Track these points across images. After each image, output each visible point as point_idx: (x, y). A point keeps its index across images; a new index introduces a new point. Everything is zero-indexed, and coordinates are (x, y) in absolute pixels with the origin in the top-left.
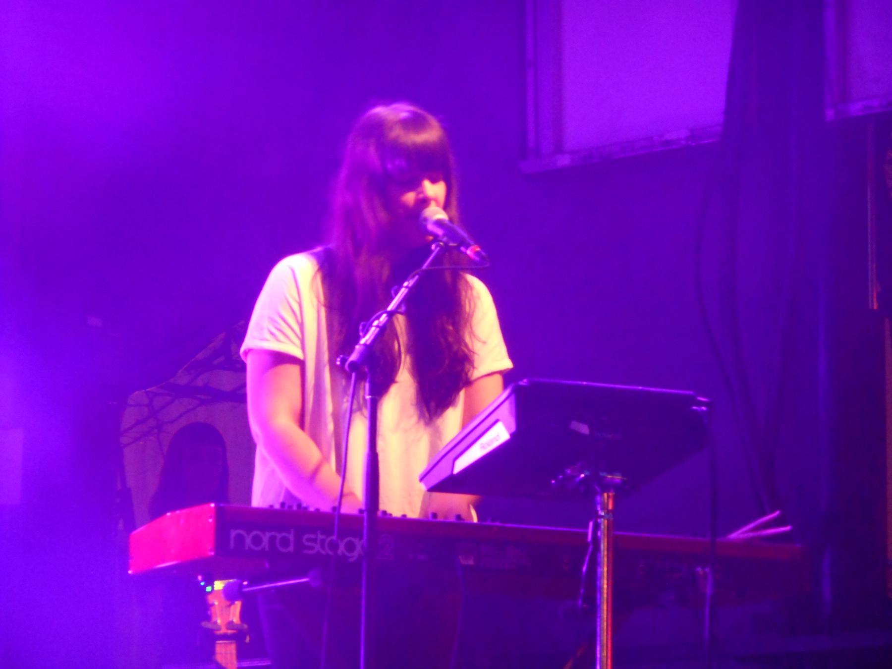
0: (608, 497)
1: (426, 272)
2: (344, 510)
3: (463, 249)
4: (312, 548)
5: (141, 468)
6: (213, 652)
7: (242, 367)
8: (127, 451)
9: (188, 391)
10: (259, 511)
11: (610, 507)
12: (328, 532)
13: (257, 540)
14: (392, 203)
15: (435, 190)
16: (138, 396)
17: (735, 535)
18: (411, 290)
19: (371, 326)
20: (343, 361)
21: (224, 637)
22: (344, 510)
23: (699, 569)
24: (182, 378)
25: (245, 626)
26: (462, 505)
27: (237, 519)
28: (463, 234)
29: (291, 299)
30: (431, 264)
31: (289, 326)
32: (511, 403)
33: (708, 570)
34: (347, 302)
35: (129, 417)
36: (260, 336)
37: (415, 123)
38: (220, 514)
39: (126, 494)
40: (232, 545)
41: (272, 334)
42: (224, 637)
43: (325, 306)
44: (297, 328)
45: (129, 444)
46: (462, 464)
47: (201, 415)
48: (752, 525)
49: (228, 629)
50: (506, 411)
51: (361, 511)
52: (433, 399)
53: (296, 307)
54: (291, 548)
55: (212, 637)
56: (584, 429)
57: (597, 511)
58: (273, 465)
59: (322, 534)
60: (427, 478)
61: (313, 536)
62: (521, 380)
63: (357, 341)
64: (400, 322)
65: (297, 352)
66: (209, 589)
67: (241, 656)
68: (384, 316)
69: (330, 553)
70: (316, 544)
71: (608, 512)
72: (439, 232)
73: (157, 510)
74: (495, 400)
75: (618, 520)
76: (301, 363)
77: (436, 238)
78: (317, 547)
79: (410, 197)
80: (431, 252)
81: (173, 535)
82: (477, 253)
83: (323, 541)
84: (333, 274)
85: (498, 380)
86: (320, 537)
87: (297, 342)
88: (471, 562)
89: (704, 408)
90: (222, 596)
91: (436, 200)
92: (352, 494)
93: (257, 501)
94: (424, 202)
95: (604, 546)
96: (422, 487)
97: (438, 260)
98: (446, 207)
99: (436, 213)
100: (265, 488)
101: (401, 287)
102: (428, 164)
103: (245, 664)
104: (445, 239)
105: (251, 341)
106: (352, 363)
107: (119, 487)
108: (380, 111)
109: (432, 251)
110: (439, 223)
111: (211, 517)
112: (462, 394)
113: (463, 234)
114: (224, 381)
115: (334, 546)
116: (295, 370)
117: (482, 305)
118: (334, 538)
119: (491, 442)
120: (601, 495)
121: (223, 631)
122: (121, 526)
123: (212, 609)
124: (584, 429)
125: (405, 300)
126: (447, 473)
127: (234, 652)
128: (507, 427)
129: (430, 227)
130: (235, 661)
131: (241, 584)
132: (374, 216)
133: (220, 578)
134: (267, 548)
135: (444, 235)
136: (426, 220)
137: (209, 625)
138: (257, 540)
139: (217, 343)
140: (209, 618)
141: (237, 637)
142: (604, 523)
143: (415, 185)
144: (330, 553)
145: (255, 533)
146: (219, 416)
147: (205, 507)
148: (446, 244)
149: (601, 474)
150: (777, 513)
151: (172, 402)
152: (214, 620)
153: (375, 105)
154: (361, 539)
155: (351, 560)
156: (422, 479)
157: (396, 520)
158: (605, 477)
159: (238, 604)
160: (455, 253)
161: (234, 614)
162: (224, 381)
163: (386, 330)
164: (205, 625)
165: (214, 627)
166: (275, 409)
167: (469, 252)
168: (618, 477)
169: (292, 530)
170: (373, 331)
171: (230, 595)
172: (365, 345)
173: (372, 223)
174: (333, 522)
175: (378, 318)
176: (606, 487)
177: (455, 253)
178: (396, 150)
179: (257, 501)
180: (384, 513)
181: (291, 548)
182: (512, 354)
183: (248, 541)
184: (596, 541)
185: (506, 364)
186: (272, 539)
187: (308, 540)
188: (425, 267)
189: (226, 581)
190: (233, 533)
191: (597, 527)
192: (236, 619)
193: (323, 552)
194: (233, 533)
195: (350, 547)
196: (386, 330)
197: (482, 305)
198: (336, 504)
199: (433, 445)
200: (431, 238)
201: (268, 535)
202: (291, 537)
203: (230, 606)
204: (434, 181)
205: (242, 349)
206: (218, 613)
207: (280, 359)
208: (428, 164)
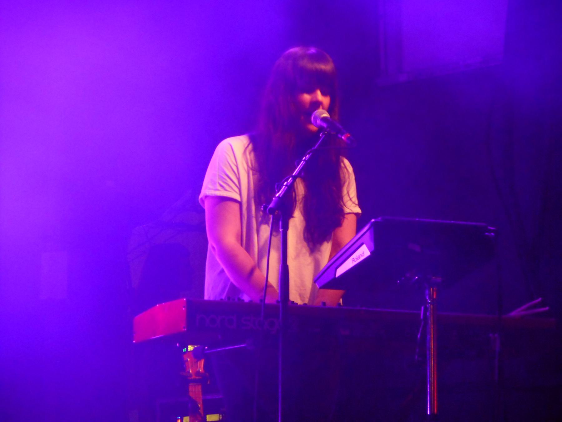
0: (433, 290)
2: (268, 301)
3: (339, 136)
10: (209, 302)
11: (435, 297)
17: (516, 313)
20: (265, 208)
21: (194, 381)
22: (294, 296)
27: (199, 310)
34: (269, 170)
36: (210, 188)
38: (190, 305)
42: (194, 381)
46: (340, 271)
48: (524, 307)
49: (196, 376)
51: (278, 301)
55: (186, 381)
64: (300, 189)
65: (238, 198)
67: (205, 391)
72: (325, 125)
74: (351, 240)
76: (240, 203)
79: (307, 97)
80: (320, 137)
82: (348, 138)
84: (258, 147)
87: (237, 190)
89: (492, 234)
92: (271, 286)
93: (208, 295)
94: (316, 104)
95: (431, 321)
98: (329, 111)
100: (211, 289)
102: (318, 81)
106: (271, 208)
110: (324, 119)
111: (184, 307)
119: (359, 257)
121: (194, 377)
123: (186, 363)
130: (201, 396)
133: (191, 344)
134: (340, 292)
141: (202, 380)
143: (311, 91)
150: (540, 299)
152: (187, 370)
161: (200, 367)
163: (291, 188)
172: (279, 196)
175: (287, 180)
179: (206, 298)
184: (426, 318)
185: (358, 210)
191: (426, 309)
199: (317, 263)
203: (197, 362)
205: (201, 196)
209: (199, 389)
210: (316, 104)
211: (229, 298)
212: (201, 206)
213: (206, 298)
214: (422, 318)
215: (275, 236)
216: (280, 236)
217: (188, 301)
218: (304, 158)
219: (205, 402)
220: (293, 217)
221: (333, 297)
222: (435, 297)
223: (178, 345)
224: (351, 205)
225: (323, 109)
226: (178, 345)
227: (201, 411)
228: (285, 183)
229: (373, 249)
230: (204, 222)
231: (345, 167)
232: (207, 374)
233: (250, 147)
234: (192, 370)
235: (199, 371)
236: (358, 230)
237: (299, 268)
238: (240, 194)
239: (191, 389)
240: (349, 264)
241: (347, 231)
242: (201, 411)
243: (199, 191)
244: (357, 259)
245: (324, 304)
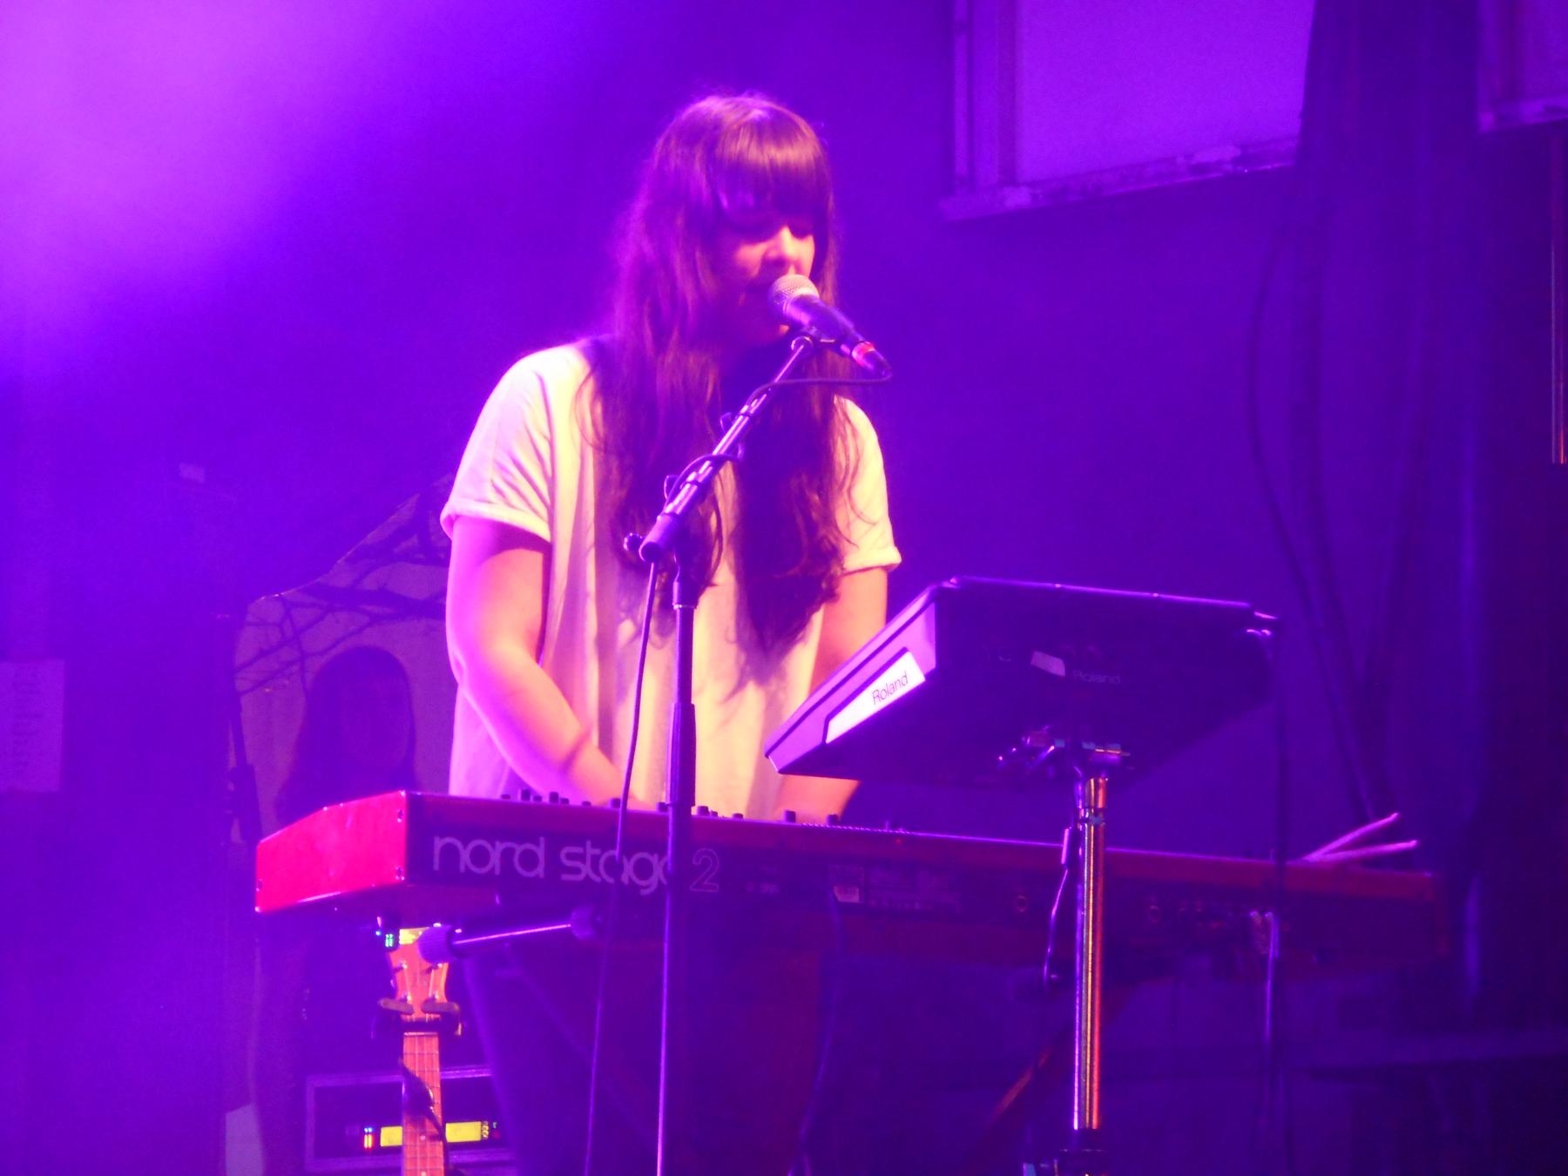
1: (782, 390)
3: (844, 348)
4: (577, 871)
5: (269, 734)
6: (399, 1052)
7: (438, 554)
8: (246, 701)
9: (350, 599)
11: (1100, 805)
12: (605, 843)
13: (480, 856)
14: (722, 262)
15: (796, 247)
16: (266, 607)
17: (1316, 856)
18: (753, 419)
19: (683, 481)
20: (635, 543)
21: (419, 1026)
22: (631, 806)
23: (1255, 915)
24: (341, 576)
26: (822, 798)
27: (436, 817)
29: (538, 427)
30: (787, 376)
32: (927, 620)
33: (1269, 915)
34: (640, 442)
35: (248, 643)
38: (416, 808)
39: (245, 774)
41: (499, 491)
42: (419, 1026)
43: (596, 448)
45: (246, 692)
46: (841, 725)
47: (372, 638)
52: (770, 625)
55: (396, 1026)
56: (1056, 667)
57: (1078, 811)
58: (489, 728)
59: (593, 846)
60: (775, 752)
61: (579, 850)
62: (948, 579)
63: (659, 510)
65: (541, 529)
66: (389, 942)
67: (446, 1061)
69: (611, 880)
70: (584, 865)
71: (1097, 811)
72: (804, 318)
73: (300, 801)
74: (872, 641)
75: (1114, 826)
76: (547, 549)
77: (796, 328)
78: (586, 869)
81: (345, 841)
82: (869, 356)
83: (595, 859)
86: (591, 851)
87: (543, 511)
88: (855, 899)
89: (1267, 632)
90: (418, 952)
94: (777, 265)
95: (1088, 871)
98: (816, 276)
99: (797, 286)
101: (736, 413)
102: (783, 200)
103: (453, 1075)
104: (813, 331)
106: (650, 545)
107: (232, 762)
108: (713, 106)
109: (791, 353)
110: (803, 303)
111: (400, 815)
112: (818, 619)
114: (409, 581)
115: (614, 867)
116: (536, 558)
117: (860, 443)
118: (616, 853)
119: (894, 687)
120: (1085, 782)
121: (417, 1014)
122: (236, 835)
123: (398, 976)
124: (1056, 667)
125: (745, 437)
126: (817, 741)
128: (919, 662)
129: (788, 309)
130: (437, 1068)
131: (452, 931)
132: (691, 282)
134: (497, 872)
135: (811, 323)
136: (780, 296)
137: (392, 1005)
138: (480, 856)
139: (405, 512)
140: (392, 993)
141: (441, 1026)
142: (1089, 832)
143: (765, 231)
144: (611, 880)
146: (400, 640)
147: (391, 796)
149: (1086, 746)
151: (321, 618)
152: (400, 995)
153: (703, 96)
154: (662, 854)
155: (644, 892)
157: (725, 821)
158: (1092, 751)
159: (443, 967)
160: (831, 356)
161: (435, 987)
162: (409, 581)
163: (705, 490)
165: (402, 1008)
166: (496, 631)
168: (1114, 752)
169: (542, 839)
170: (686, 493)
171: (430, 951)
172: (672, 514)
173: (690, 296)
174: (614, 824)
175: (697, 467)
176: (1095, 768)
177: (831, 356)
178: (737, 174)
179: (458, 787)
180: (704, 810)
181: (540, 871)
182: (900, 541)
183: (465, 856)
184: (1075, 863)
185: (893, 556)
186: (507, 855)
187: (570, 856)
189: (420, 931)
190: (439, 843)
191: (1077, 839)
192: (440, 996)
193: (594, 877)
194: (439, 843)
195: (644, 869)
196: (705, 490)
197: (860, 443)
198: (619, 794)
199: (772, 706)
200: (785, 328)
201: (500, 846)
202: (540, 852)
203: (429, 971)
204: (798, 234)
205: (444, 515)
206: (408, 983)
207: (508, 538)
208: (783, 200)
209: (432, 1046)
210: (777, 265)
212: (445, 536)
213: (458, 787)
214: (1063, 860)
215: (660, 648)
216: (675, 637)
217: (410, 797)
218: (745, 408)
219: (446, 1085)
220: (713, 585)
221: (822, 798)
222: (1100, 805)
224: (869, 539)
225: (799, 270)
227: (436, 1110)
228: (691, 477)
229: (932, 664)
230: (443, 593)
231: (855, 433)
232: (456, 1007)
233: (575, 801)
234: (414, 993)
235: (433, 998)
236: (892, 611)
237: (731, 730)
240: (863, 708)
241: (860, 610)
242: (436, 1110)
243: (445, 499)
244: (888, 693)
245: (791, 816)
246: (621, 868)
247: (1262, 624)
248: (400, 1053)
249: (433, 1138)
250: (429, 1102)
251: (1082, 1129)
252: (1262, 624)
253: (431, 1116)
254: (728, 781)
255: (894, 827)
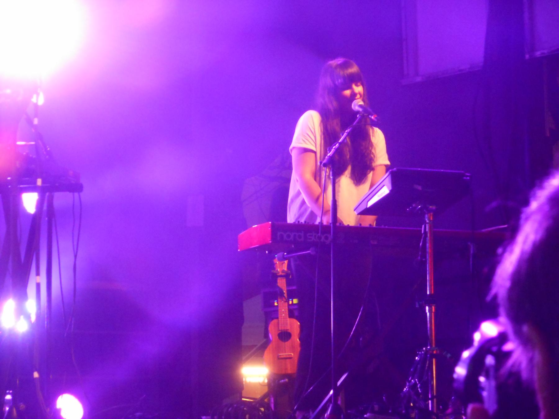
4: (311, 239)
6: (276, 282)
10: (291, 224)
13: (289, 236)
15: (359, 89)
19: (332, 148)
21: (281, 276)
25: (289, 272)
28: (370, 110)
31: (310, 137)
37: (345, 65)
40: (278, 239)
42: (281, 276)
44: (314, 139)
46: (371, 203)
50: (388, 182)
53: (313, 130)
54: (302, 239)
55: (275, 276)
56: (419, 188)
65: (313, 148)
67: (288, 284)
68: (337, 144)
72: (361, 110)
75: (434, 225)
79: (347, 92)
80: (357, 117)
83: (315, 236)
85: (384, 168)
86: (314, 234)
87: (314, 144)
88: (376, 243)
91: (360, 94)
93: (291, 218)
96: (356, 213)
97: (360, 120)
105: (295, 143)
110: (360, 106)
113: (370, 110)
115: (320, 238)
117: (378, 138)
119: (381, 195)
121: (280, 274)
124: (419, 188)
127: (285, 282)
128: (388, 188)
137: (275, 272)
138: (289, 236)
140: (274, 269)
141: (286, 276)
145: (288, 233)
148: (363, 115)
156: (355, 210)
164: (273, 271)
167: (372, 117)
175: (335, 145)
176: (429, 211)
181: (302, 239)
182: (390, 159)
185: (388, 163)
186: (295, 235)
188: (354, 124)
190: (279, 234)
192: (285, 269)
195: (326, 238)
197: (378, 138)
202: (302, 234)
205: (291, 147)
207: (306, 150)
211: (305, 222)
221: (370, 220)
223: (267, 252)
226: (267, 252)
227: (285, 295)
229: (391, 188)
238: (316, 147)
239: (278, 281)
242: (285, 295)
246: (321, 238)
247: (467, 176)
248: (277, 282)
249: (285, 302)
250: (284, 293)
251: (430, 294)
252: (467, 176)
253: (284, 296)
254: (349, 217)
255: (385, 226)
